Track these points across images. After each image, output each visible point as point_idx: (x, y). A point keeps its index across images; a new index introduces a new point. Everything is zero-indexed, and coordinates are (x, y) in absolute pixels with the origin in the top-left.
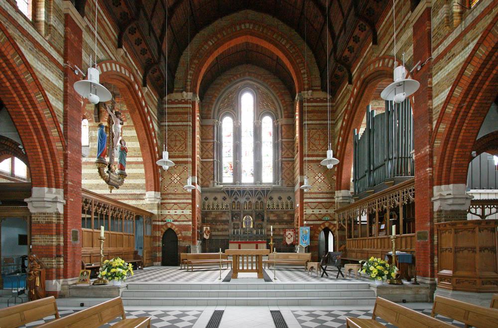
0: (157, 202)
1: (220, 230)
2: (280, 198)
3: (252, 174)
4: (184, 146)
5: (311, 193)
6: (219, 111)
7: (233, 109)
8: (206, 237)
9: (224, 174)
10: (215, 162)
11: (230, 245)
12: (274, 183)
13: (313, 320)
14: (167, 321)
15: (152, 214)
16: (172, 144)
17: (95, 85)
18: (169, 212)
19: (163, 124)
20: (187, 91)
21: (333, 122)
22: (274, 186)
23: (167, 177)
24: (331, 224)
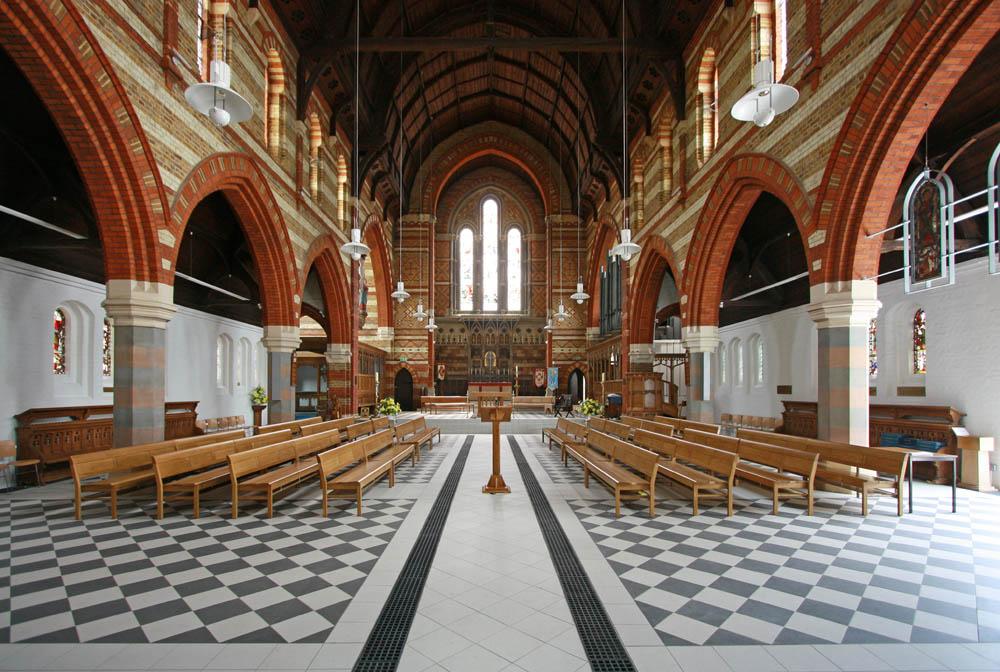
5: (559, 329)
6: (456, 222)
9: (462, 300)
12: (522, 312)
13: (612, 523)
14: (349, 525)
15: (385, 352)
16: (408, 272)
17: (222, 91)
20: (423, 213)
21: (584, 250)
24: (581, 365)
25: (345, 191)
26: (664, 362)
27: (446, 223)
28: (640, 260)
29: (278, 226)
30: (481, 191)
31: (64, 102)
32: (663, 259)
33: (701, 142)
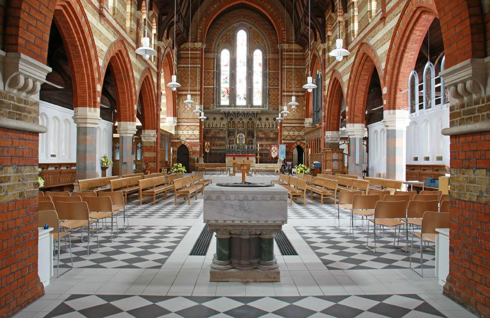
0: (174, 125)
2: (215, 119)
3: (245, 98)
4: (194, 82)
6: (218, 45)
7: (230, 44)
8: (207, 151)
10: (215, 89)
11: (226, 157)
12: (263, 106)
15: (171, 134)
22: (262, 109)
24: (301, 143)
25: (155, 39)
26: (346, 142)
27: (212, 46)
28: (398, 24)
29: (129, 69)
30: (235, 25)
31: (74, 40)
33: (354, 27)
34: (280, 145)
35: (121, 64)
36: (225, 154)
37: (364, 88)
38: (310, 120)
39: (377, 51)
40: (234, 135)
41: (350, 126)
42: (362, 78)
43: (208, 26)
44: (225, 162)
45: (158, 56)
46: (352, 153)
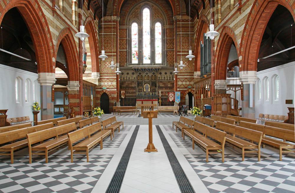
0: (98, 78)
1: (131, 92)
3: (149, 58)
6: (130, 20)
7: (138, 19)
8: (123, 97)
9: (133, 58)
10: (128, 52)
12: (162, 64)
15: (96, 85)
16: (106, 45)
18: (104, 84)
19: (100, 34)
23: (103, 64)
24: (192, 90)
27: (125, 20)
29: (44, 24)
30: (142, 4)
32: (230, 38)
34: (176, 92)
35: (34, 17)
36: (136, 99)
37: (259, 37)
38: (199, 73)
39: (235, 32)
40: (142, 86)
41: (244, 74)
42: (258, 27)
43: (121, 3)
44: (135, 105)
45: (79, 21)
46: (245, 98)
